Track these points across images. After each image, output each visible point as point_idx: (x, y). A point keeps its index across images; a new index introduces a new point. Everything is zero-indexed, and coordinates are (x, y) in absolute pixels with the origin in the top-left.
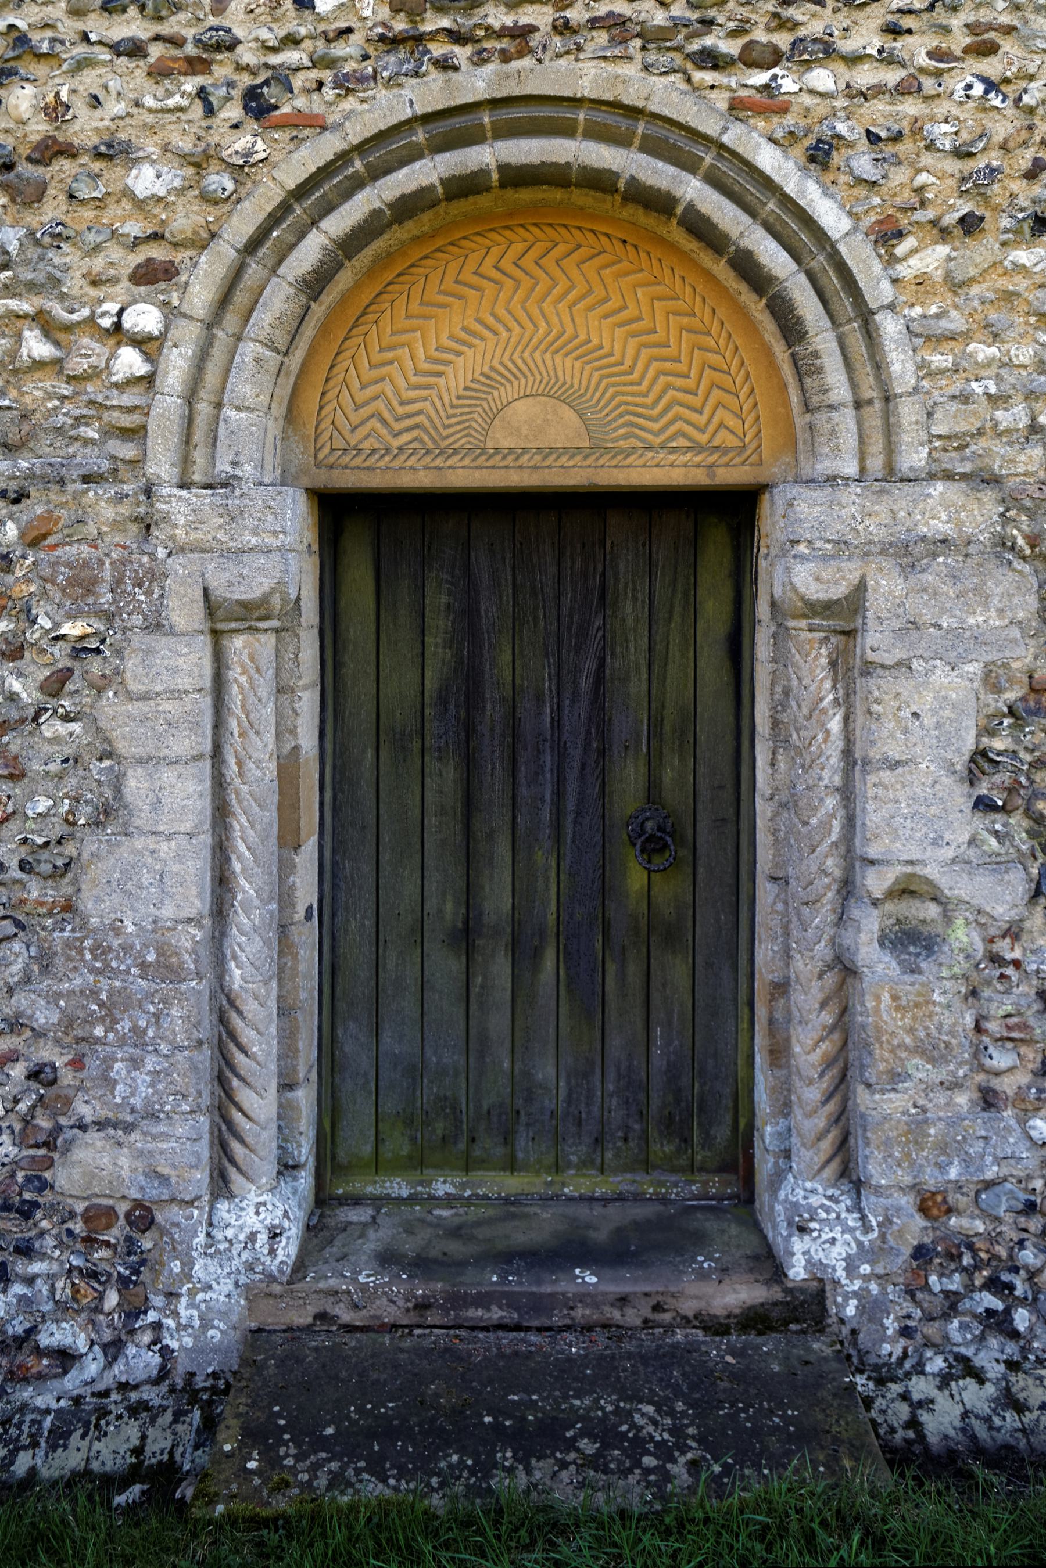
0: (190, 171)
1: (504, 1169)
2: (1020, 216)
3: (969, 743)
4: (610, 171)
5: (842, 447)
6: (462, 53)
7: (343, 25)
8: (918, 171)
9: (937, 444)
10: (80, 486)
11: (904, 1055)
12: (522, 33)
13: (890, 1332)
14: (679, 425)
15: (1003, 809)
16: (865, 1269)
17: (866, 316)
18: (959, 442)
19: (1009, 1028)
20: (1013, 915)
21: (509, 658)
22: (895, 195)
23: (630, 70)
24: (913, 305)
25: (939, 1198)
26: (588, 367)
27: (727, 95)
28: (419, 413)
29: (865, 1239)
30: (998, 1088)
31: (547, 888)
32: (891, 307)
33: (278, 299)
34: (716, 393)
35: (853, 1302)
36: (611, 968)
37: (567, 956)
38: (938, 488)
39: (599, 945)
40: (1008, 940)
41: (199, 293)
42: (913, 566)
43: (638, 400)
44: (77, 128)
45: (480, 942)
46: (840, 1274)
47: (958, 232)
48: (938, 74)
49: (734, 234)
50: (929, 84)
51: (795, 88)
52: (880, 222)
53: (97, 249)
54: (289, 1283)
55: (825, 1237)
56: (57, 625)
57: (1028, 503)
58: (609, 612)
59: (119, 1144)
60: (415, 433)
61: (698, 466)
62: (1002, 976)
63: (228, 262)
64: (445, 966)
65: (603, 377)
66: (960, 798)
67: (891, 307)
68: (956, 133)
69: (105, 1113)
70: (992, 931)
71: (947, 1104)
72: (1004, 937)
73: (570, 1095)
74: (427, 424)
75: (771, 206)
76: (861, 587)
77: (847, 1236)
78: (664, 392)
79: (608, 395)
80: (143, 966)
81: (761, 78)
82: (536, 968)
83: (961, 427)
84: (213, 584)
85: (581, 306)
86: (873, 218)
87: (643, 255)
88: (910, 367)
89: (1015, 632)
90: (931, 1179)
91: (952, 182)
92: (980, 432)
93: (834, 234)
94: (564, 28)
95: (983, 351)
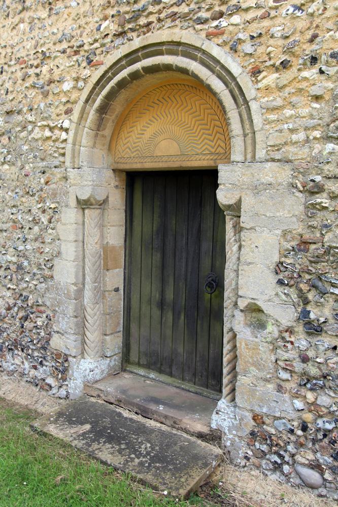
0: (75, 82)
1: (169, 375)
2: (305, 58)
3: (276, 258)
4: (170, 64)
5: (236, 151)
6: (134, 34)
7: (106, 33)
8: (268, 47)
9: (269, 148)
10: (54, 169)
11: (249, 365)
12: (149, 24)
13: (240, 455)
14: (206, 146)
15: (287, 285)
16: (234, 432)
17: (246, 102)
18: (277, 148)
19: (286, 365)
20: (289, 324)
21: (175, 222)
22: (259, 58)
23: (177, 30)
24: (264, 97)
25: (260, 417)
26: (181, 129)
27: (205, 32)
28: (138, 146)
29: (235, 422)
30: (284, 386)
31: (183, 294)
32: (255, 99)
33: (92, 115)
34: (218, 134)
35: (229, 441)
36: (199, 322)
37: (186, 316)
38: (269, 164)
39: (196, 314)
40: (288, 333)
41: (75, 115)
42: (258, 193)
43: (194, 138)
44: (54, 75)
45: (165, 307)
46: (226, 431)
47: (281, 68)
48: (276, 8)
49: (204, 79)
50: (273, 13)
51: (227, 24)
52: (253, 68)
53: (57, 107)
54: (92, 384)
55: (222, 418)
56: (50, 205)
57: (302, 170)
58: (202, 209)
59: (61, 338)
60: (137, 152)
61: (212, 160)
62: (284, 346)
63: (81, 106)
64: (156, 312)
65: (185, 131)
66: (273, 279)
67: (255, 99)
68: (283, 29)
69: (58, 330)
70: (281, 329)
71: (264, 386)
72: (286, 331)
73: (187, 358)
74: (140, 149)
75: (218, 68)
76: (240, 201)
77: (229, 420)
78: (202, 135)
79: (186, 137)
80: (64, 294)
81: (215, 23)
82: (179, 318)
83: (278, 142)
84: (78, 195)
85: (180, 109)
86: (250, 67)
87: (201, 92)
88: (260, 120)
89: (294, 219)
90: (257, 410)
91: (281, 49)
92: (286, 143)
93: (236, 75)
94: (159, 20)
95: (288, 112)
